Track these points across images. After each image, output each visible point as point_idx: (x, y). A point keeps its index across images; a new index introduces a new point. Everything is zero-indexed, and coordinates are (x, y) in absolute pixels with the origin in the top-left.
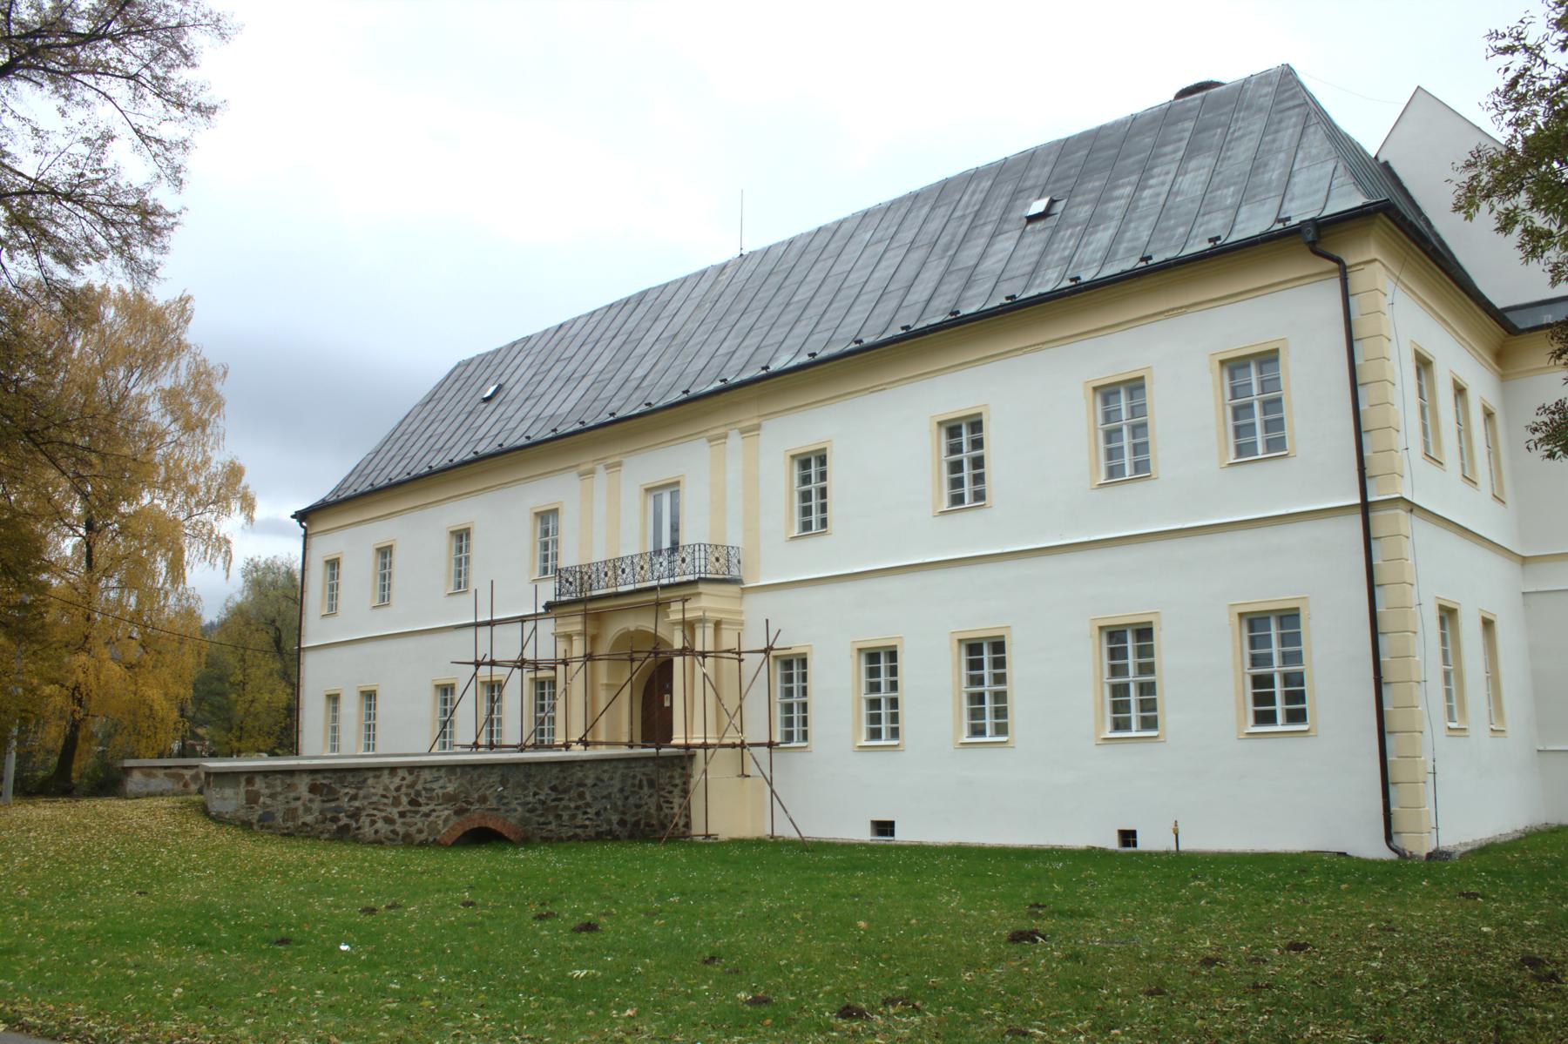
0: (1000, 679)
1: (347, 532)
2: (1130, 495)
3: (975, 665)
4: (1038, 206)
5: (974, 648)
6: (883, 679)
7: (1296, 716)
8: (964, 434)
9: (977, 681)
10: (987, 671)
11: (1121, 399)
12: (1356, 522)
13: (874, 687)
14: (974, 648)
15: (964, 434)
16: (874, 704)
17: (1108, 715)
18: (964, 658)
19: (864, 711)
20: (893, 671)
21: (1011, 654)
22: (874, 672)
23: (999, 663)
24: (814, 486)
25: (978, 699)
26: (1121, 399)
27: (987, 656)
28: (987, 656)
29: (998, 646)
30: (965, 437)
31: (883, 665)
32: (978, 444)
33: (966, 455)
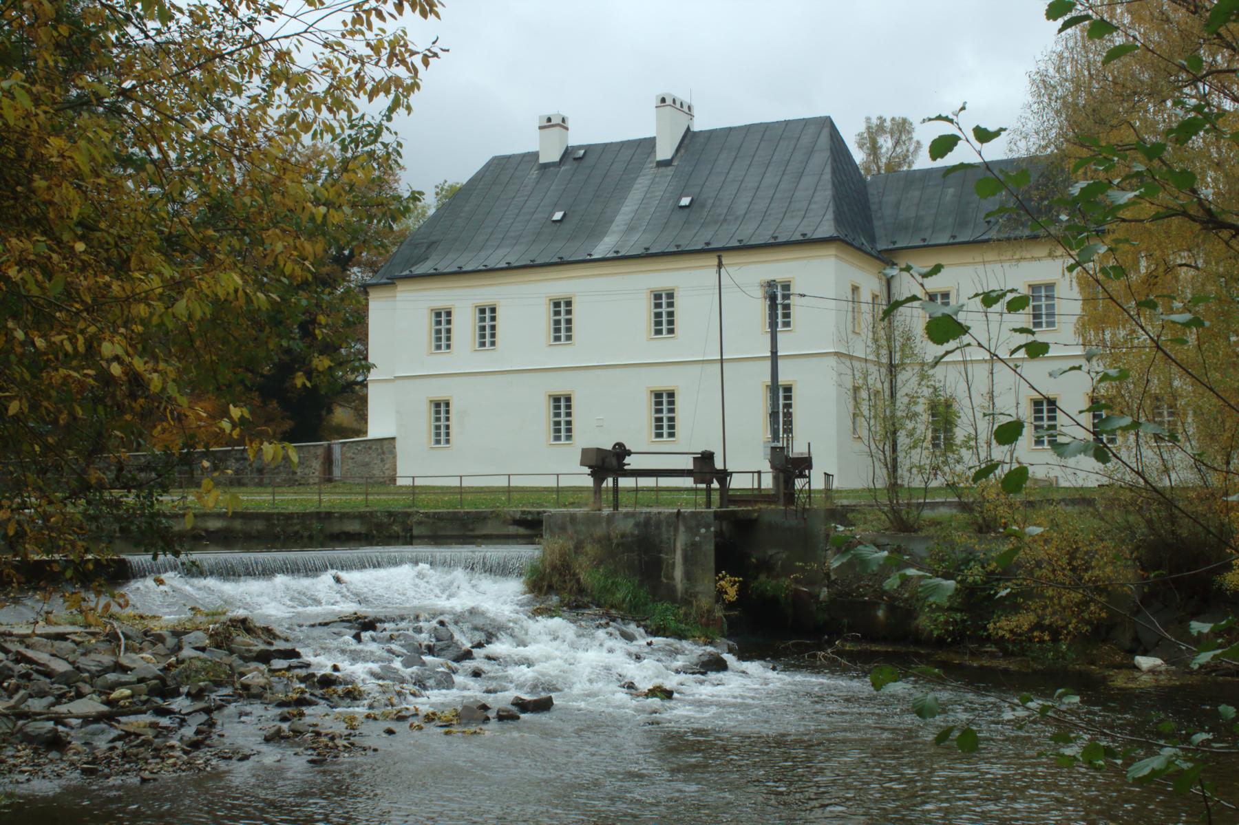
0: (672, 410)
1: (682, 272)
2: (665, 341)
3: (557, 407)
4: (558, 216)
5: (557, 399)
6: (443, 415)
7: (672, 435)
8: (562, 309)
9: (557, 415)
10: (563, 411)
11: (442, 317)
12: (719, 365)
13: (438, 419)
14: (557, 399)
15: (562, 309)
16: (438, 427)
17: (552, 434)
18: (552, 404)
19: (433, 431)
20: (447, 412)
21: (574, 403)
22: (438, 412)
23: (672, 403)
24: (443, 327)
25: (558, 423)
26: (442, 317)
27: (563, 404)
28: (563, 404)
29: (671, 395)
30: (488, 315)
31: (443, 408)
32: (569, 312)
33: (488, 323)
